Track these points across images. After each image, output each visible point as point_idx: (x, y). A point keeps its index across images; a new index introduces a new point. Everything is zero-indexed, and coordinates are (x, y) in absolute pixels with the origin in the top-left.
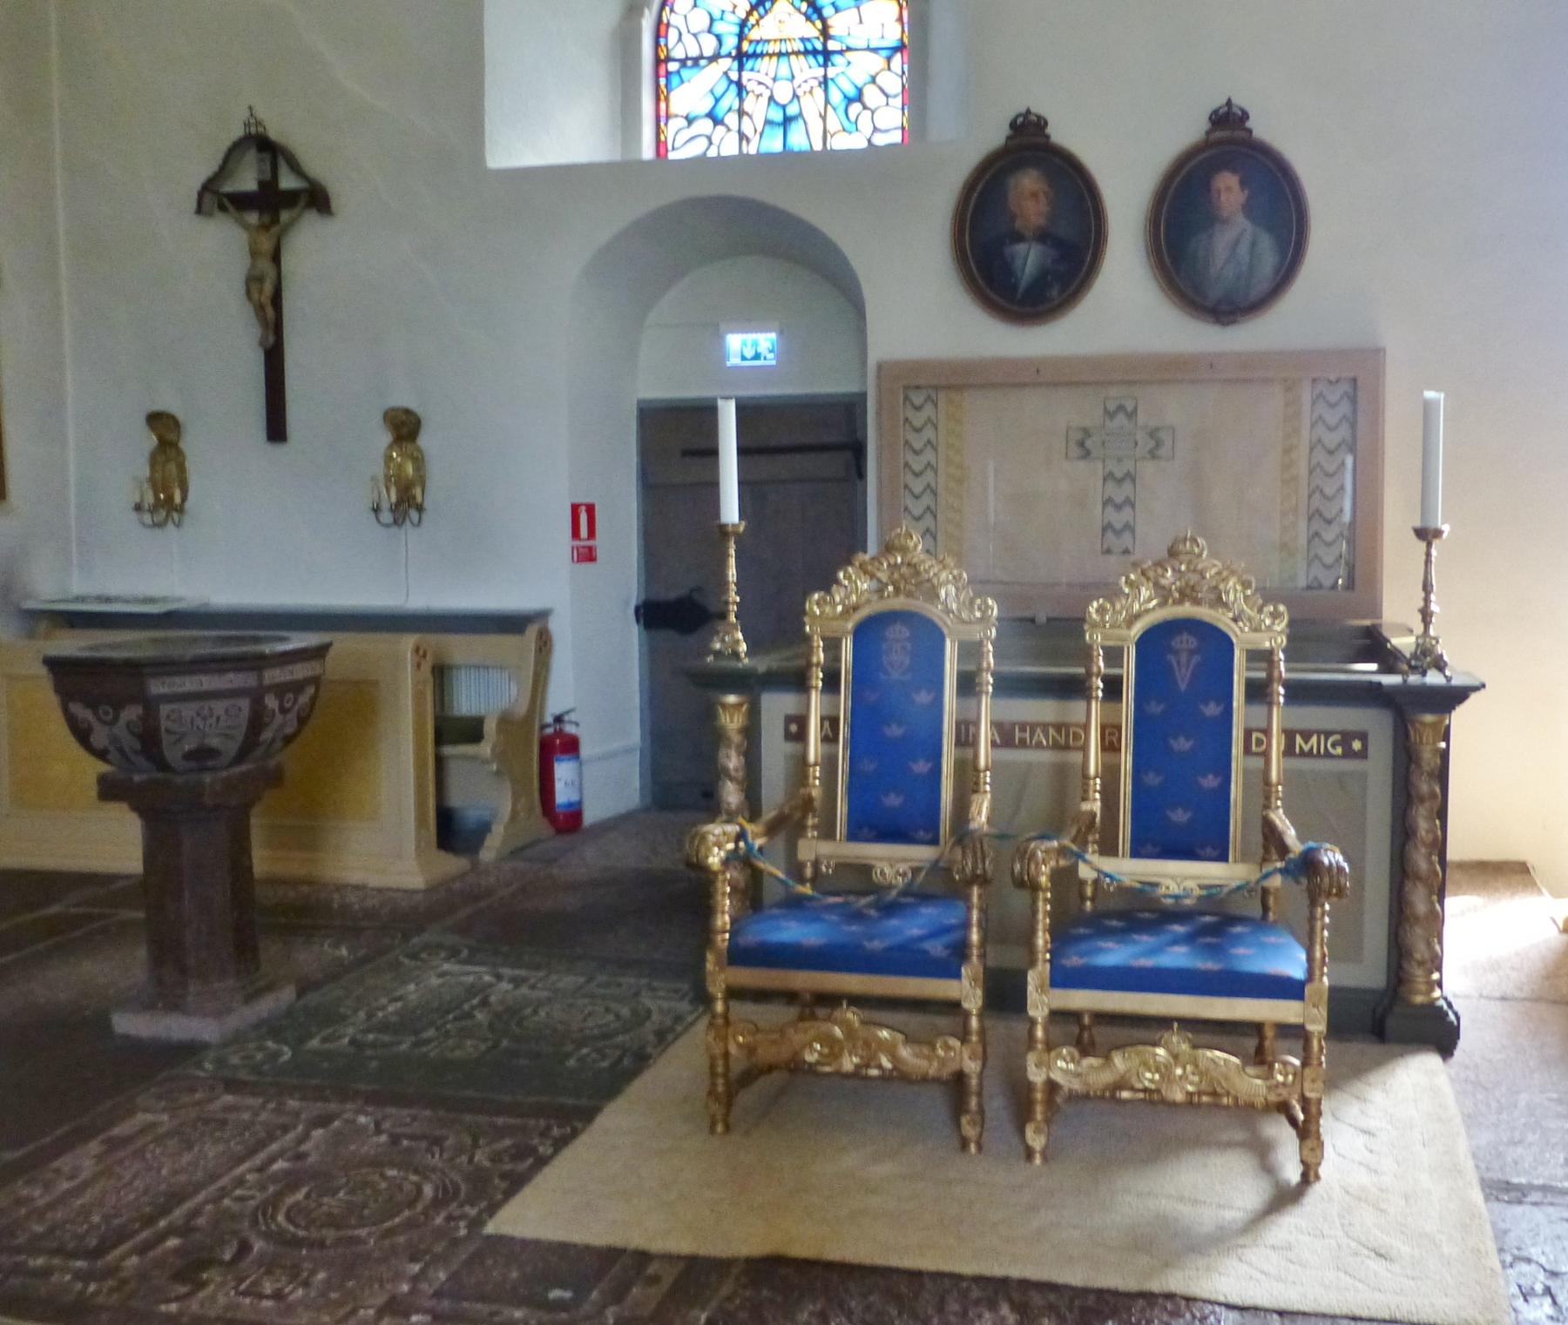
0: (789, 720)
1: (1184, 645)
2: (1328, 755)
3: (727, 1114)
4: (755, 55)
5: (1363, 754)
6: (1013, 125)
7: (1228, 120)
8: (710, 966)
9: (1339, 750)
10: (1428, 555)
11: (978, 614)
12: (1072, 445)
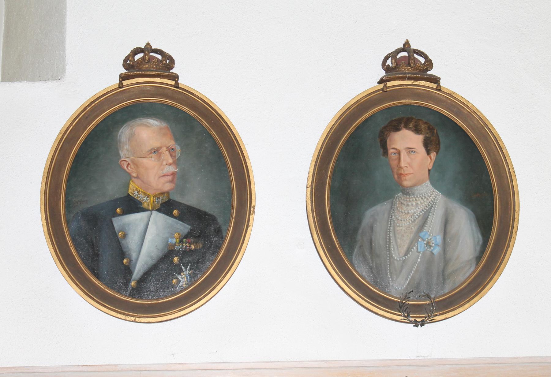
7: (408, 64)
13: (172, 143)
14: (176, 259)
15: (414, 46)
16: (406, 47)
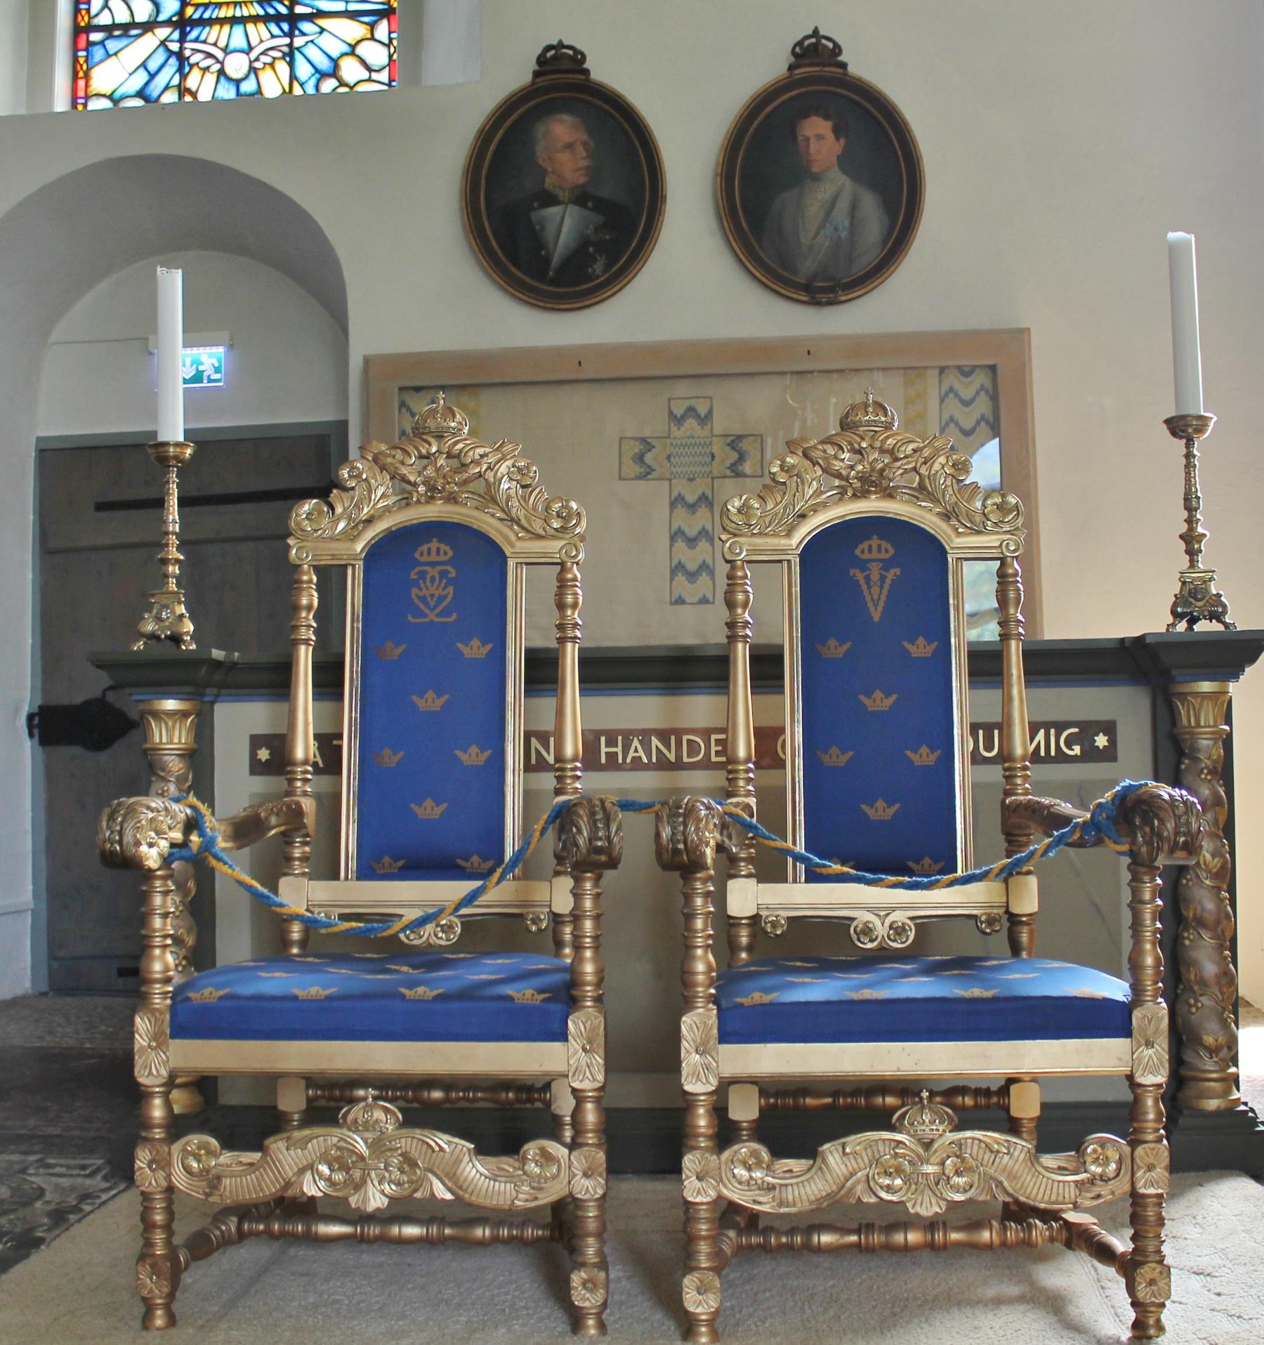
0: (257, 741)
1: (875, 555)
2: (1061, 758)
3: (171, 1296)
4: (202, 22)
5: (1109, 755)
6: (541, 60)
7: (815, 53)
8: (141, 1041)
9: (1077, 750)
10: (1189, 456)
11: (556, 524)
12: (627, 460)
13: (585, 137)
14: (591, 249)
15: (822, 33)
16: (816, 32)
